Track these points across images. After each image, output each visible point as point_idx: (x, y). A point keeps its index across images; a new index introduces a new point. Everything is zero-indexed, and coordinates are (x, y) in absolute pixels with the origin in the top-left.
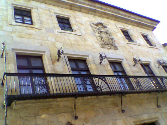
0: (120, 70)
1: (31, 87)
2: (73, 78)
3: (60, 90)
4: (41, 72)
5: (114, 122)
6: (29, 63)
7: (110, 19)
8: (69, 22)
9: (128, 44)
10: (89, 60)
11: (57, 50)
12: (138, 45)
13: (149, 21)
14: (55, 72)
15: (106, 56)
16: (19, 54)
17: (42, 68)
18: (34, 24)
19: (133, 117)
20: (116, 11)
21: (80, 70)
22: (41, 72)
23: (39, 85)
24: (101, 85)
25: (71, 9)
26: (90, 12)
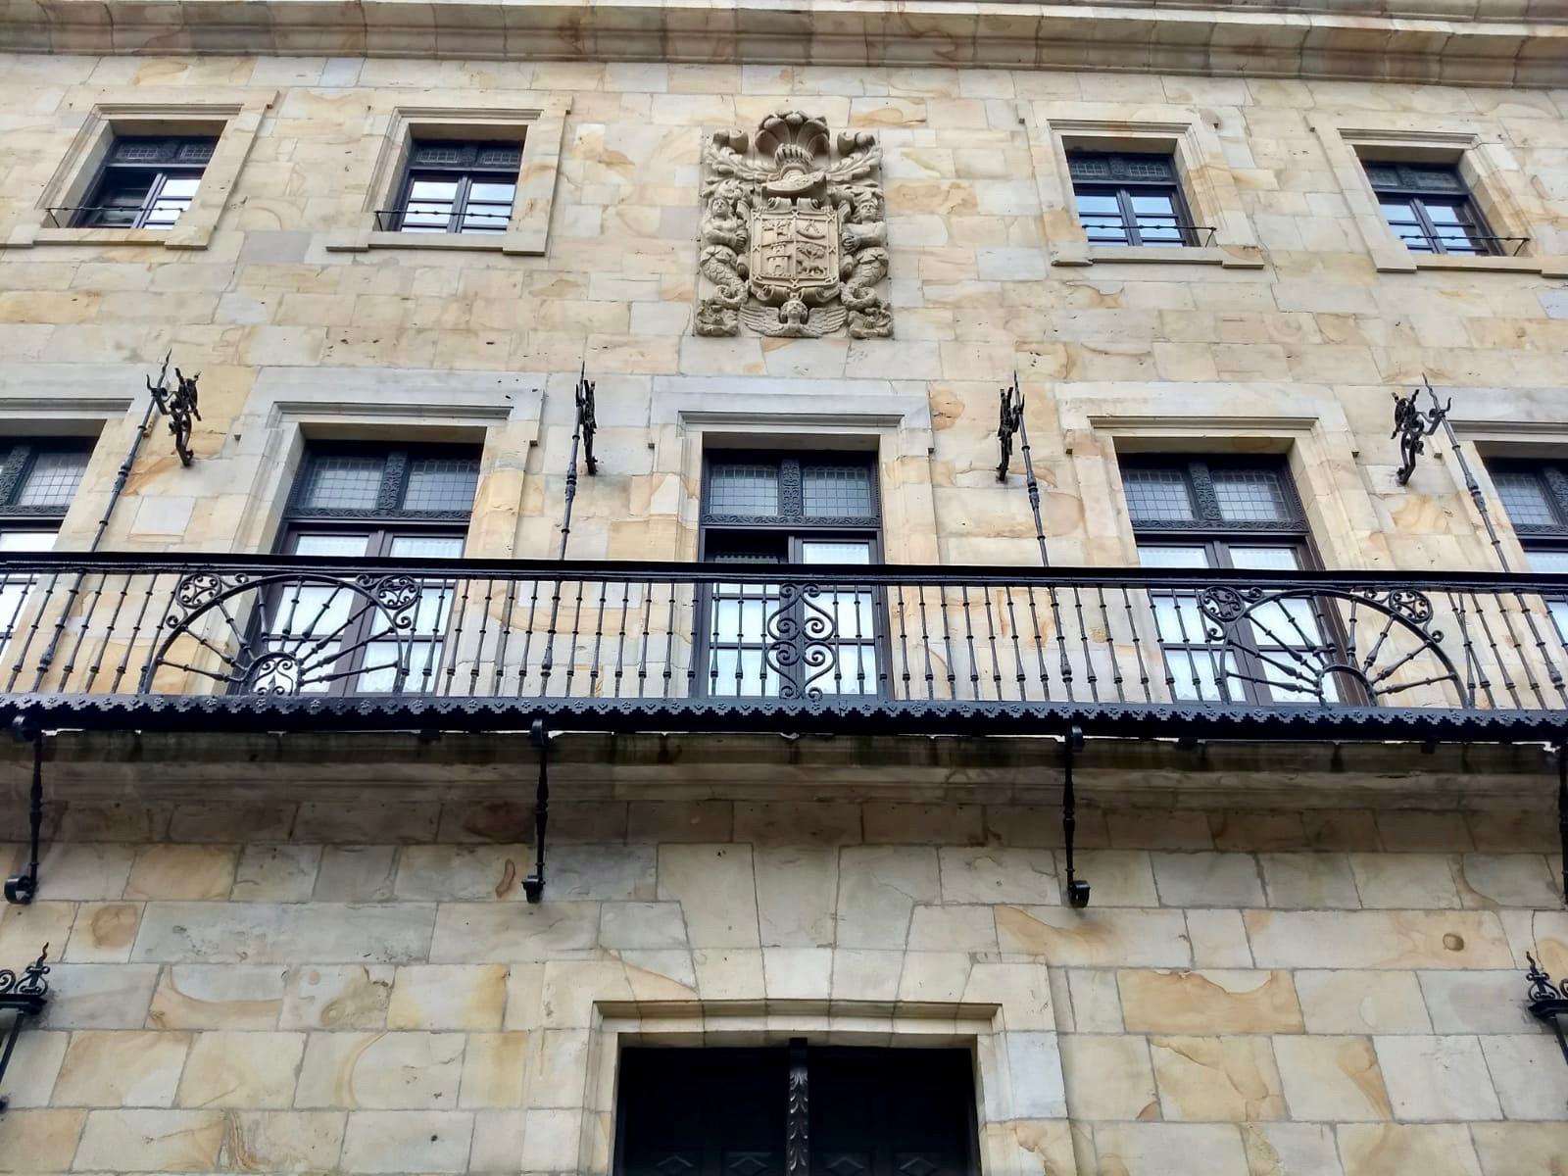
2: (1533, 600)
4: (857, 555)
5: (379, 973)
6: (1202, 504)
9: (1068, 274)
12: (1218, 263)
14: (1393, 558)
15: (1443, 406)
17: (868, 533)
18: (1202, 234)
21: (1225, 539)
22: (857, 555)
24: (1370, 661)
25: (576, 57)
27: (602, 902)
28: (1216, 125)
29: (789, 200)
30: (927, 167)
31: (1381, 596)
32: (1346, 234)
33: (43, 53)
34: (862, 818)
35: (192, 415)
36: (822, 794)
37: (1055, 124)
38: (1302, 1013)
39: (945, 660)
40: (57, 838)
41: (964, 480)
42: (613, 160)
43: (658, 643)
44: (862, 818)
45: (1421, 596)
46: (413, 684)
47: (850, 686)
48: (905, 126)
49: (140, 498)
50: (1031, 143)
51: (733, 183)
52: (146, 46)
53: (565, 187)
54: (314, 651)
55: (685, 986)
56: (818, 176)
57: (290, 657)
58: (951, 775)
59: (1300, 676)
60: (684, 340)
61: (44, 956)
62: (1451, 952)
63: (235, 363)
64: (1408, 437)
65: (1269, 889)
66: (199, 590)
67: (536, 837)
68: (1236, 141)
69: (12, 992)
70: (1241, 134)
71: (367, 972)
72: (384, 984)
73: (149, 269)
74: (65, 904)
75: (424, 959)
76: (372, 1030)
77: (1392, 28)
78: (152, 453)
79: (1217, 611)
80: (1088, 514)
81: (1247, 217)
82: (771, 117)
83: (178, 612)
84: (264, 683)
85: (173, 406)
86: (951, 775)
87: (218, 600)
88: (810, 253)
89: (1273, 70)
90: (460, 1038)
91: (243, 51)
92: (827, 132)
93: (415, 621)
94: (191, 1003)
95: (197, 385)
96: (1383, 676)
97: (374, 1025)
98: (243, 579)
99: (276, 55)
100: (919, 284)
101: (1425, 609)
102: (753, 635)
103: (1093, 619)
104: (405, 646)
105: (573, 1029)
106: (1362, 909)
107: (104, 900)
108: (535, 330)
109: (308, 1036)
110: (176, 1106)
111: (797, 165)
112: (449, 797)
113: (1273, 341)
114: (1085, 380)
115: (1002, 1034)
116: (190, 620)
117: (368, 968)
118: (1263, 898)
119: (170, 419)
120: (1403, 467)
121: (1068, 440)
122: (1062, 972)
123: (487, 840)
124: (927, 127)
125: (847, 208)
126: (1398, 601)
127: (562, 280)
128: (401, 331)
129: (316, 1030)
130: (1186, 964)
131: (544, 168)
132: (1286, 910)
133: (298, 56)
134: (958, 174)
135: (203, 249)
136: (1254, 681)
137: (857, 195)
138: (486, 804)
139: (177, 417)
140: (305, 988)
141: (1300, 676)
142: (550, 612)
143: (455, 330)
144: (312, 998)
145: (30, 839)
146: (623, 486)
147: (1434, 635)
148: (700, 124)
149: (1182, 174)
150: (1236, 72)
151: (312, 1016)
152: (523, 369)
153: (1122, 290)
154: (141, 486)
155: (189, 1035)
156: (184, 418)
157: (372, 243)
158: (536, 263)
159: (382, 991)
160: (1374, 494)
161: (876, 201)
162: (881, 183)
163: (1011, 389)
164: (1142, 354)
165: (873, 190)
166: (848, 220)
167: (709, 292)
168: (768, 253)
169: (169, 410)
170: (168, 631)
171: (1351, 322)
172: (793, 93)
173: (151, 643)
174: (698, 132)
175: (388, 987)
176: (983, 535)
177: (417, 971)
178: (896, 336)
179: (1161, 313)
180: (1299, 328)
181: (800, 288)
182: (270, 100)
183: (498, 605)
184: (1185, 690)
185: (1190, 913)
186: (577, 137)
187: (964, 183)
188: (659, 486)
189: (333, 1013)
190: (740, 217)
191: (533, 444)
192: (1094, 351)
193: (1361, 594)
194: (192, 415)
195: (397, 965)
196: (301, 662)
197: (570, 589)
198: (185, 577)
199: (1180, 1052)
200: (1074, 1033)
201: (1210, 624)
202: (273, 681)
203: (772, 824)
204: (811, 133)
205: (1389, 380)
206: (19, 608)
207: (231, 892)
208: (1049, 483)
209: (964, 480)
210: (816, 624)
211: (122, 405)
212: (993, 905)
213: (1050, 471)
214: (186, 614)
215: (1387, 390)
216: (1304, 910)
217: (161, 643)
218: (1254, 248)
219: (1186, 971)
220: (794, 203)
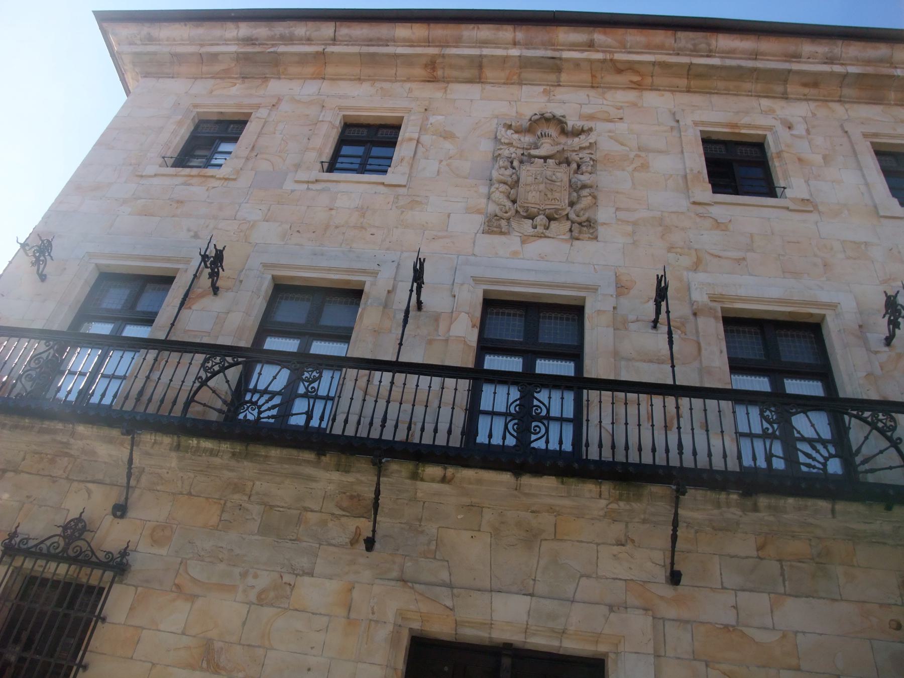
0: (520, 343)
1: (85, 380)
3: (613, 447)
4: (566, 368)
5: (287, 578)
7: (653, 88)
8: (880, 161)
9: (700, 209)
10: (833, 331)
11: (885, 298)
13: (507, 33)
16: (732, 315)
17: (575, 354)
18: (779, 191)
19: (410, 584)
20: (685, 39)
22: (566, 368)
23: (548, 418)
26: (528, 75)
27: (406, 556)
28: (789, 128)
29: (542, 160)
30: (622, 144)
31: (867, 414)
32: (862, 194)
33: (169, 77)
34: (556, 524)
35: (220, 268)
36: (533, 508)
37: (696, 124)
38: (799, 658)
39: (611, 432)
40: (138, 486)
41: (632, 326)
42: (448, 136)
43: (446, 412)
44: (556, 524)
45: (890, 415)
46: (314, 423)
47: (553, 446)
48: (610, 121)
49: (191, 311)
50: (682, 134)
51: (512, 150)
52: (217, 73)
53: (421, 150)
54: (267, 402)
55: (447, 607)
56: (559, 148)
57: (255, 403)
58: (609, 504)
59: (814, 459)
60: (478, 235)
61: (128, 547)
62: (894, 631)
63: (244, 241)
64: (892, 318)
65: (787, 583)
66: (214, 364)
67: (373, 516)
68: (800, 137)
69: (111, 563)
70: (804, 133)
71: (282, 577)
72: (290, 585)
73: (207, 190)
74: (139, 521)
75: (311, 574)
76: (282, 608)
77: (896, 74)
78: (199, 288)
79: (770, 417)
80: (703, 352)
81: (805, 181)
82: (536, 114)
83: (203, 375)
84: (241, 416)
85: (212, 263)
86: (609, 504)
87: (223, 369)
88: (552, 190)
89: (824, 96)
90: (325, 619)
91: (264, 76)
92: (566, 123)
93: (318, 389)
94: (194, 580)
95: (224, 253)
96: (865, 462)
97: (282, 606)
98: (235, 359)
99: (279, 78)
100: (613, 210)
101: (892, 424)
102: (501, 407)
103: (698, 416)
104: (312, 401)
105: (385, 622)
106: (842, 600)
107: (157, 522)
108: (397, 227)
109: (250, 606)
110: (183, 634)
111: (549, 141)
112: (329, 488)
113: (815, 255)
114: (706, 271)
115: (623, 653)
116: (208, 379)
117: (282, 574)
118: (783, 588)
119: (209, 270)
120: (888, 335)
121: (695, 307)
122: (661, 621)
123: (348, 514)
124: (623, 122)
125: (574, 166)
126: (877, 418)
127: (414, 200)
128: (327, 227)
129: (254, 604)
130: (734, 623)
131: (411, 139)
132: (796, 596)
133: (291, 79)
134: (639, 149)
135: (234, 180)
136: (790, 456)
137: (581, 159)
138: (348, 494)
139: (212, 270)
140: (250, 581)
141: (814, 459)
142: (389, 388)
143: (355, 227)
144: (253, 587)
145: (125, 485)
146: (436, 318)
147: (897, 439)
148: (497, 117)
149: (769, 155)
150: (802, 97)
151: (253, 596)
152: (388, 249)
153: (730, 221)
154: (193, 304)
155: (193, 598)
156: (216, 270)
157: (317, 179)
158: (401, 191)
159: (288, 588)
160: (871, 351)
161: (592, 163)
162: (596, 152)
163: (662, 276)
164: (740, 259)
165: (591, 156)
166: (576, 172)
167: (492, 208)
168: (528, 188)
169: (209, 265)
170: (197, 384)
171: (863, 246)
172: (549, 101)
173: (190, 388)
174: (496, 121)
175: (292, 586)
176: (641, 361)
177: (307, 579)
178: (599, 238)
179: (752, 236)
180: (832, 249)
181: (545, 209)
182: (274, 101)
183: (362, 382)
184: (747, 462)
185: (739, 593)
186: (429, 123)
187: (643, 154)
188: (455, 320)
189: (263, 597)
190: (513, 168)
191: (389, 292)
192: (712, 255)
193: (855, 412)
194: (220, 268)
195: (297, 575)
196: (260, 407)
197: (400, 377)
198: (208, 356)
199: (724, 674)
200: (665, 656)
201: (766, 425)
202: (246, 416)
203: (503, 523)
204: (559, 122)
205: (885, 282)
206: (129, 368)
207: (218, 526)
208: (682, 332)
209: (632, 326)
210: (537, 410)
211: (188, 261)
212: (625, 580)
213: (683, 324)
214: (207, 375)
215: (882, 288)
216: (807, 597)
217: (194, 389)
218: (808, 200)
219: (733, 626)
220: (545, 162)
